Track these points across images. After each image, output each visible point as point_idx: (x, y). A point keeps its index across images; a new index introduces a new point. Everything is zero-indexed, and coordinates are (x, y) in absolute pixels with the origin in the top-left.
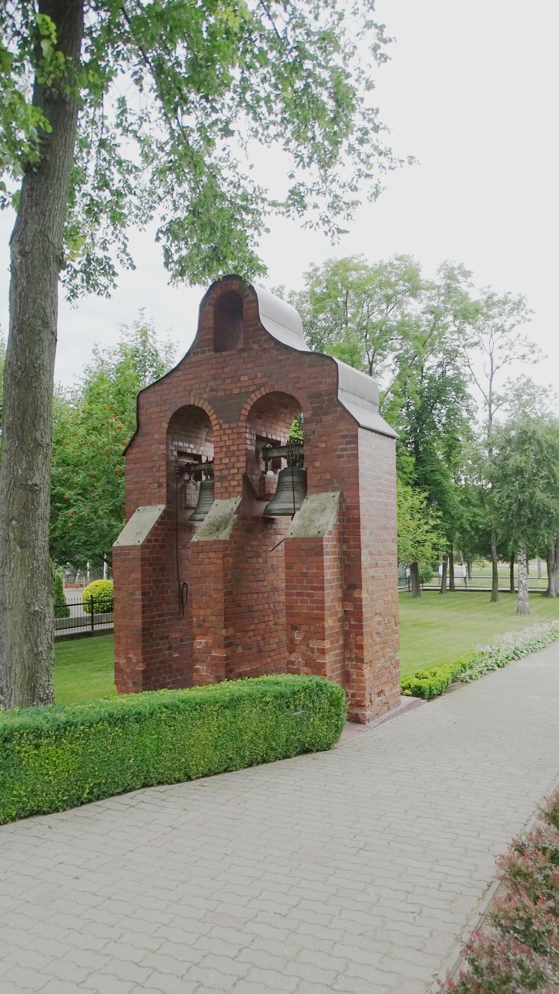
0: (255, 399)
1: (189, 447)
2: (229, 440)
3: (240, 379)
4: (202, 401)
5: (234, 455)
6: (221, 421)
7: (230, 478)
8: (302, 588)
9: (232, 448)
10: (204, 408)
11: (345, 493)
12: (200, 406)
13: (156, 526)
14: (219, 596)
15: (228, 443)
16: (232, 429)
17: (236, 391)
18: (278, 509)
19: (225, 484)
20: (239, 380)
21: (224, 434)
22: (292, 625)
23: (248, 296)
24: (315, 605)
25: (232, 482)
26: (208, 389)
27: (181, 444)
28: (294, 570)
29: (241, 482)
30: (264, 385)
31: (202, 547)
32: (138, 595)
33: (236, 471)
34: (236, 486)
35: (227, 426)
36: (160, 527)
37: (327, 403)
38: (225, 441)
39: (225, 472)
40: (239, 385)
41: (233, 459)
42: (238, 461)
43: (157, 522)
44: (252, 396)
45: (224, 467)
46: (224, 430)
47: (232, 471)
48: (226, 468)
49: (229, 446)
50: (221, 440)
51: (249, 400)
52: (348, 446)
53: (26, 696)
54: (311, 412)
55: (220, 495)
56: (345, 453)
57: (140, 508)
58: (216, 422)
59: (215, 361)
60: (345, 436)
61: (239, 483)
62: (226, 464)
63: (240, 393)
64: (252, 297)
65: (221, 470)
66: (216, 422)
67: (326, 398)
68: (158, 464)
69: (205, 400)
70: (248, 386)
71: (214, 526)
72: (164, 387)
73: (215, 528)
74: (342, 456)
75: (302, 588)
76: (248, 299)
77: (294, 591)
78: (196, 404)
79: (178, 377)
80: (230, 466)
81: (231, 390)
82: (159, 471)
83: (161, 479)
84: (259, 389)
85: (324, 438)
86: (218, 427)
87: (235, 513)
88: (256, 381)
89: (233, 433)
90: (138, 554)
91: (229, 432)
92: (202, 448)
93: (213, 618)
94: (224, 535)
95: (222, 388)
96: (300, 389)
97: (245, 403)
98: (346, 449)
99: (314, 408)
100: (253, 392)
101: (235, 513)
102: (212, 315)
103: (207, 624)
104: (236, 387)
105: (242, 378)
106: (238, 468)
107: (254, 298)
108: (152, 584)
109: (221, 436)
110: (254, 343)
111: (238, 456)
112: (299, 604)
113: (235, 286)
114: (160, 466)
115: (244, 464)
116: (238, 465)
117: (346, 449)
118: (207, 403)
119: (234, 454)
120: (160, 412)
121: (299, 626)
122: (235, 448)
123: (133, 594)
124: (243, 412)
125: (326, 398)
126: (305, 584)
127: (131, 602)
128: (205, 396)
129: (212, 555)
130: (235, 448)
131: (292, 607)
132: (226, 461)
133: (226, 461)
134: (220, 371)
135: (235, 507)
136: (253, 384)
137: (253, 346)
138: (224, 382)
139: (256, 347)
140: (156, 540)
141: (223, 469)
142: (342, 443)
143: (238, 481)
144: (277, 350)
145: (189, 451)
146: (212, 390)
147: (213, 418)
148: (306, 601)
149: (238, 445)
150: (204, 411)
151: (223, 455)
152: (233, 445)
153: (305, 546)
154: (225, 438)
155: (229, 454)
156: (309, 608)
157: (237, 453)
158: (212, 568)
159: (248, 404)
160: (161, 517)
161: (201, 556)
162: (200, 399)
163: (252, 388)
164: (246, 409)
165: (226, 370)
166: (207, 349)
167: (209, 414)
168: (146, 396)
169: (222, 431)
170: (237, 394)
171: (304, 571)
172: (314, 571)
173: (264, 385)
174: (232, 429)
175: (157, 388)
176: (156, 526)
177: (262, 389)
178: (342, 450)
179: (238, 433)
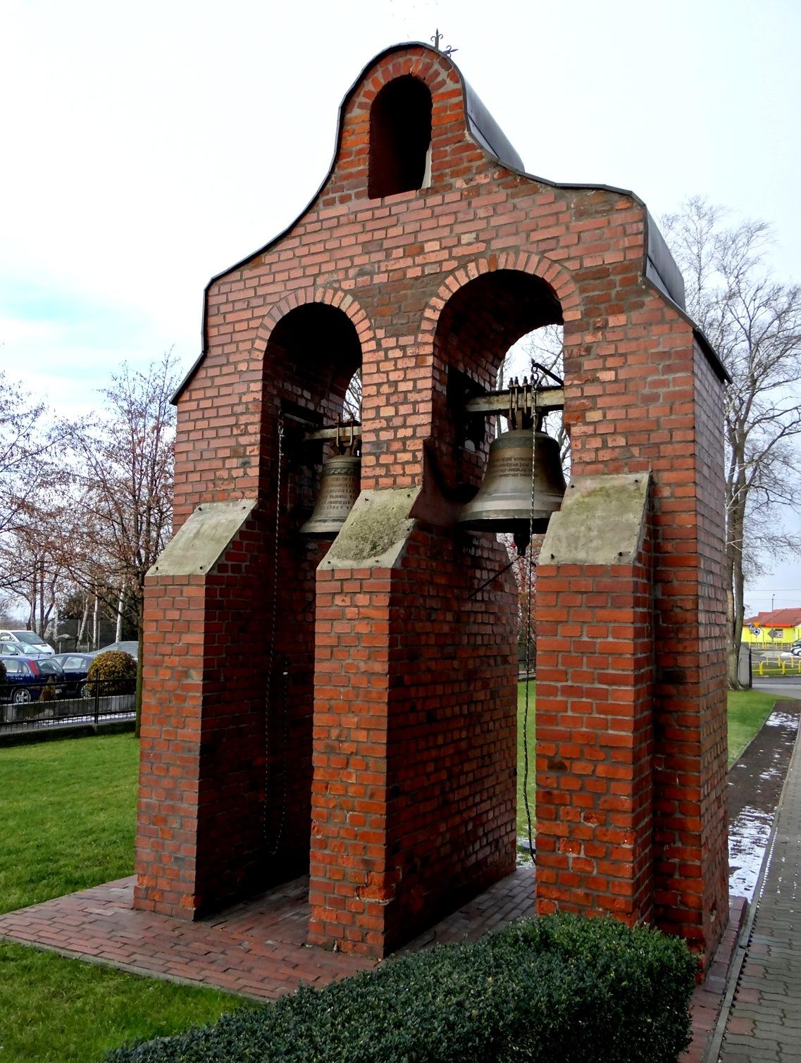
0: (455, 288)
1: (302, 396)
2: (396, 369)
3: (422, 248)
4: (340, 294)
5: (405, 402)
6: (380, 333)
7: (396, 446)
8: (578, 676)
9: (403, 387)
10: (343, 308)
11: (665, 477)
12: (335, 305)
13: (238, 539)
14: (730, 749)
15: (394, 376)
16: (403, 348)
17: (411, 273)
18: (496, 511)
19: (384, 459)
20: (421, 251)
21: (387, 359)
22: (550, 759)
23: (443, 83)
24: (609, 717)
25: (399, 455)
26: (352, 272)
27: (288, 386)
28: (559, 638)
29: (420, 455)
30: (475, 258)
31: (345, 580)
32: (196, 678)
33: (409, 432)
34: (408, 462)
35: (391, 342)
36: (245, 543)
37: (618, 289)
38: (387, 373)
39: (384, 436)
40: (419, 260)
41: (404, 410)
42: (415, 413)
43: (240, 532)
44: (450, 280)
45: (384, 424)
46: (386, 350)
47: (402, 433)
48: (388, 428)
49: (396, 382)
50: (378, 371)
51: (442, 288)
52: (670, 377)
53: (126, 466)
54: (582, 308)
55: (372, 482)
56: (662, 391)
57: (202, 506)
58: (369, 334)
59: (369, 215)
60: (664, 355)
61: (415, 456)
62: (388, 419)
63: (423, 276)
64: (451, 86)
65: (376, 431)
66: (369, 334)
67: (618, 278)
68: (243, 420)
69: (346, 292)
70: (440, 263)
71: (365, 539)
72: (264, 270)
73: (368, 547)
74: (655, 398)
75: (578, 676)
76: (442, 90)
77: (559, 684)
78: (327, 302)
79: (292, 249)
80: (398, 421)
81: (404, 270)
82: (245, 433)
83: (249, 449)
84: (463, 266)
85: (610, 362)
86: (372, 345)
87: (410, 516)
88: (457, 252)
89: (405, 356)
90: (199, 593)
91: (398, 353)
92: (324, 402)
93: (362, 736)
94: (389, 559)
95: (383, 269)
96: (555, 261)
97: (432, 295)
98: (664, 383)
99: (589, 301)
100: (452, 272)
101: (410, 516)
102: (367, 126)
103: (347, 747)
104: (415, 265)
105: (429, 247)
106: (415, 427)
107: (459, 86)
108: (224, 656)
109: (378, 363)
110: (455, 174)
111: (415, 403)
112: (570, 713)
113: (415, 65)
114: (246, 425)
115: (427, 419)
116: (412, 421)
117: (664, 383)
118: (349, 299)
119: (406, 398)
120: (253, 318)
121: (567, 763)
122: (409, 386)
123: (186, 674)
124: (428, 313)
125: (618, 278)
126: (585, 669)
127: (179, 692)
128: (348, 285)
129: (362, 599)
130: (409, 386)
131: (552, 720)
132: (388, 412)
133: (388, 412)
134: (381, 234)
135: (409, 503)
136: (451, 258)
137: (452, 181)
138: (388, 256)
139: (459, 183)
140: (236, 569)
141: (382, 429)
142: (656, 371)
143: (414, 452)
144: (506, 187)
145: (302, 403)
146: (362, 273)
147: (362, 328)
148: (589, 708)
149: (415, 380)
150: (344, 314)
151: (381, 401)
152: (405, 380)
153: (587, 583)
154: (389, 366)
155: (394, 399)
156: (592, 723)
157: (413, 397)
158: (363, 628)
159: (438, 297)
160: (247, 523)
161: (338, 601)
162: (336, 290)
163: (448, 266)
164: (434, 308)
165: (393, 232)
166: (352, 192)
167: (355, 320)
168: (225, 289)
169: (382, 354)
170: (417, 278)
171: (585, 639)
172: (610, 639)
173: (475, 258)
174: (403, 348)
175: (247, 273)
176: (238, 539)
177: (472, 266)
178: (656, 384)
179: (417, 356)
